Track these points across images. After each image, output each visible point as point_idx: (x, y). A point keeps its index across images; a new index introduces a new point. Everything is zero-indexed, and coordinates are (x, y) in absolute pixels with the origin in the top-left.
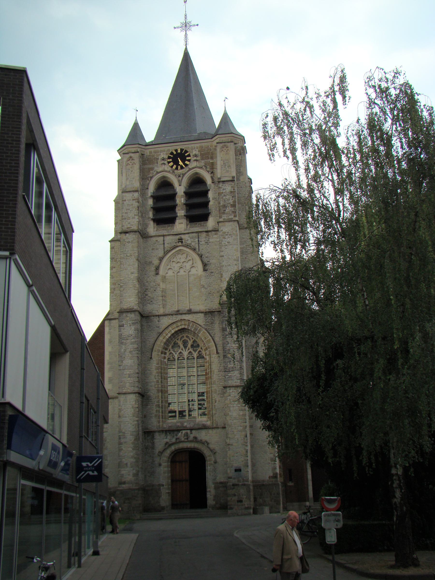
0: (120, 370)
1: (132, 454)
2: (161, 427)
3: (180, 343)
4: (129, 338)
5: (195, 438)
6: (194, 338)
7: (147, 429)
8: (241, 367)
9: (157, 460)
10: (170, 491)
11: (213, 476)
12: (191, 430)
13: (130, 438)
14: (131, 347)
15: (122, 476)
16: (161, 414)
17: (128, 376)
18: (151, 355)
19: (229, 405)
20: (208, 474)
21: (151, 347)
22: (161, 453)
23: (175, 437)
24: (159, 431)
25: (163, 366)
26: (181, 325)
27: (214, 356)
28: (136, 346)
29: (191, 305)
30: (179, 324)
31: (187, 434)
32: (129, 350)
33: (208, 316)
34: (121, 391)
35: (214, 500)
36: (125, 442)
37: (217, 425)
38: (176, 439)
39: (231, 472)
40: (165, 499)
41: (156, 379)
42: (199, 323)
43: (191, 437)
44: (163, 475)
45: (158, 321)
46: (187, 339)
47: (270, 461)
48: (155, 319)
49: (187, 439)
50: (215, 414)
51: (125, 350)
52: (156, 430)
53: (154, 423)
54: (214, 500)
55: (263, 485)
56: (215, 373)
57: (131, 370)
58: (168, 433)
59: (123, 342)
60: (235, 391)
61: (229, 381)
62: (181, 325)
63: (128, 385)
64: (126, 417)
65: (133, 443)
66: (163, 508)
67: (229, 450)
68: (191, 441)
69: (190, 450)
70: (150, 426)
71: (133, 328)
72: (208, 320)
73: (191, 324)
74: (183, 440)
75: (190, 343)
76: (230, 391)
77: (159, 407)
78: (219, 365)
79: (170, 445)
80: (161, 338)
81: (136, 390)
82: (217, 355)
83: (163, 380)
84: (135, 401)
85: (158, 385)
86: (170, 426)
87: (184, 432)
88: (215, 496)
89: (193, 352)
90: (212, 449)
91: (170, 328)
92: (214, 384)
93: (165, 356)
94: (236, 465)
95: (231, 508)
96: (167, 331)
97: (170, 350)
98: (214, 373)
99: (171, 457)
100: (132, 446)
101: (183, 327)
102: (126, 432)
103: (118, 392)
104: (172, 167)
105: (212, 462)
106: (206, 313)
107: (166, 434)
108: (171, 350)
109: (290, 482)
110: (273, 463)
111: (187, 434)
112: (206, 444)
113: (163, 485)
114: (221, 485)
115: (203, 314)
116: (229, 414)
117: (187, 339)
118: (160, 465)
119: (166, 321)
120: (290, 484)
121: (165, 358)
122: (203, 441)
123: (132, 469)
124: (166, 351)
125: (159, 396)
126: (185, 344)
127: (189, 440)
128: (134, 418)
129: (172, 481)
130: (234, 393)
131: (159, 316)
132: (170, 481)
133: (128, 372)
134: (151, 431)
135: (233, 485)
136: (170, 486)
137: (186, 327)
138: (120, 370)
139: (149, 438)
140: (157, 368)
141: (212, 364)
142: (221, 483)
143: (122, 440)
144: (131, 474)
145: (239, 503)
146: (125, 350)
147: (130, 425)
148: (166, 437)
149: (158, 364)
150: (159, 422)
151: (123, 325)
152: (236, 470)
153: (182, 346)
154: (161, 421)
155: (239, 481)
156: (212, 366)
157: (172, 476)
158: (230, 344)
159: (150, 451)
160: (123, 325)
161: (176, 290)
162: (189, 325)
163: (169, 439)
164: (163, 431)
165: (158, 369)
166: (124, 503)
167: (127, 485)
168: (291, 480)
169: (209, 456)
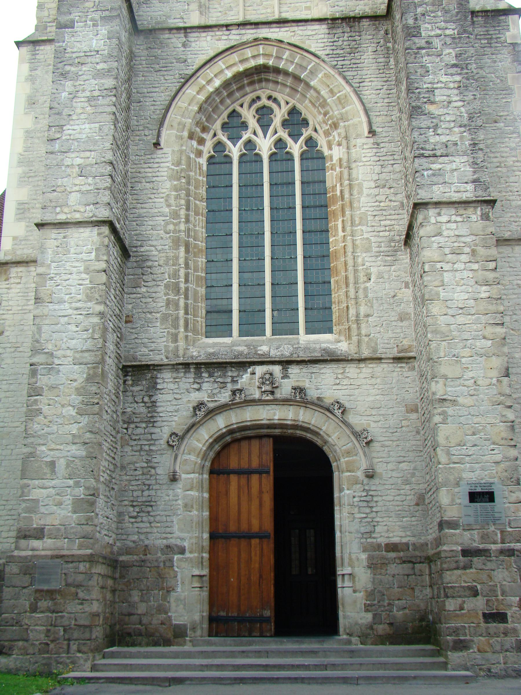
0: (52, 153)
1: (74, 429)
2: (181, 353)
3: (249, 116)
4: (89, 60)
5: (300, 390)
6: (292, 102)
7: (135, 359)
8: (475, 144)
9: (164, 463)
10: (206, 572)
11: (364, 522)
12: (286, 363)
13: (70, 374)
14: (92, 85)
15: (34, 506)
16: (182, 312)
17: (76, 170)
18: (159, 136)
19: (439, 265)
20: (345, 514)
21: (157, 116)
22: (177, 439)
23: (230, 386)
24: (175, 367)
25: (192, 174)
26: (254, 57)
27: (359, 141)
28: (109, 82)
29: (283, 10)
30: (248, 53)
31: (269, 379)
32: (88, 94)
33: (340, 31)
34: (49, 217)
35: (367, 608)
36: (52, 388)
37: (375, 351)
38: (234, 392)
39: (451, 502)
40: (187, 600)
41: (169, 206)
42: (312, 50)
43: (286, 388)
44: (182, 515)
45: (184, 45)
46: (270, 103)
48: (174, 40)
49: (271, 396)
50: (368, 316)
51: (73, 96)
52: (166, 361)
53: (157, 342)
54: (367, 608)
56: (365, 192)
57: (88, 154)
58: (205, 375)
59: (68, 72)
60: (459, 219)
61: (435, 188)
62: (254, 57)
63: (74, 198)
64: (61, 302)
65: (79, 391)
66: (179, 634)
67: (444, 422)
68: (286, 402)
69: (277, 431)
70: (145, 350)
71: (103, 31)
72: (340, 43)
73: (287, 53)
74: (257, 395)
75: (279, 114)
76: (439, 219)
77: (178, 292)
78: (377, 169)
79: (212, 413)
80: (190, 91)
81: (104, 213)
82: (371, 140)
83: (192, 213)
84: (97, 250)
85: (175, 225)
86: (213, 354)
87: (260, 370)
88: (370, 594)
89: (289, 141)
90: (358, 429)
91: (221, 64)
92: (359, 224)
93: (201, 148)
94: (475, 475)
95: (461, 645)
96: (210, 72)
97: (215, 135)
98: (360, 193)
99: (212, 454)
100: (76, 399)
101: (261, 61)
102: (59, 353)
103: (36, 221)
105: (360, 474)
106: (333, 22)
107: (198, 374)
108: (220, 133)
111: (269, 379)
112: (338, 412)
113: (182, 551)
114: (392, 555)
115: (324, 27)
116: (438, 294)
117: (270, 103)
118: (174, 479)
119: (207, 45)
121: (199, 154)
122: (328, 401)
123: (71, 482)
124: (204, 136)
125: (177, 258)
126: (264, 116)
127: (278, 395)
128: (89, 304)
129: (213, 537)
130: (454, 226)
131: (186, 30)
132: (206, 536)
133: (79, 161)
134: (147, 367)
135: (466, 553)
136: (206, 555)
137: (271, 63)
138: (52, 153)
139: (136, 389)
140: (175, 176)
141: (353, 165)
142: (392, 547)
143: (43, 381)
144: (68, 500)
145: (493, 626)
146: (73, 96)
147: (73, 328)
148: (196, 386)
149: (179, 164)
150: (175, 338)
151: (73, 22)
152: (474, 497)
153: (252, 123)
154: (181, 336)
155: (485, 538)
156: (354, 173)
157: (214, 519)
158: (434, 73)
159: (139, 431)
160: (73, 22)
162: (279, 58)
163: (210, 391)
164: (186, 365)
165: (179, 179)
166: (34, 609)
167: (48, 542)
169: (348, 453)
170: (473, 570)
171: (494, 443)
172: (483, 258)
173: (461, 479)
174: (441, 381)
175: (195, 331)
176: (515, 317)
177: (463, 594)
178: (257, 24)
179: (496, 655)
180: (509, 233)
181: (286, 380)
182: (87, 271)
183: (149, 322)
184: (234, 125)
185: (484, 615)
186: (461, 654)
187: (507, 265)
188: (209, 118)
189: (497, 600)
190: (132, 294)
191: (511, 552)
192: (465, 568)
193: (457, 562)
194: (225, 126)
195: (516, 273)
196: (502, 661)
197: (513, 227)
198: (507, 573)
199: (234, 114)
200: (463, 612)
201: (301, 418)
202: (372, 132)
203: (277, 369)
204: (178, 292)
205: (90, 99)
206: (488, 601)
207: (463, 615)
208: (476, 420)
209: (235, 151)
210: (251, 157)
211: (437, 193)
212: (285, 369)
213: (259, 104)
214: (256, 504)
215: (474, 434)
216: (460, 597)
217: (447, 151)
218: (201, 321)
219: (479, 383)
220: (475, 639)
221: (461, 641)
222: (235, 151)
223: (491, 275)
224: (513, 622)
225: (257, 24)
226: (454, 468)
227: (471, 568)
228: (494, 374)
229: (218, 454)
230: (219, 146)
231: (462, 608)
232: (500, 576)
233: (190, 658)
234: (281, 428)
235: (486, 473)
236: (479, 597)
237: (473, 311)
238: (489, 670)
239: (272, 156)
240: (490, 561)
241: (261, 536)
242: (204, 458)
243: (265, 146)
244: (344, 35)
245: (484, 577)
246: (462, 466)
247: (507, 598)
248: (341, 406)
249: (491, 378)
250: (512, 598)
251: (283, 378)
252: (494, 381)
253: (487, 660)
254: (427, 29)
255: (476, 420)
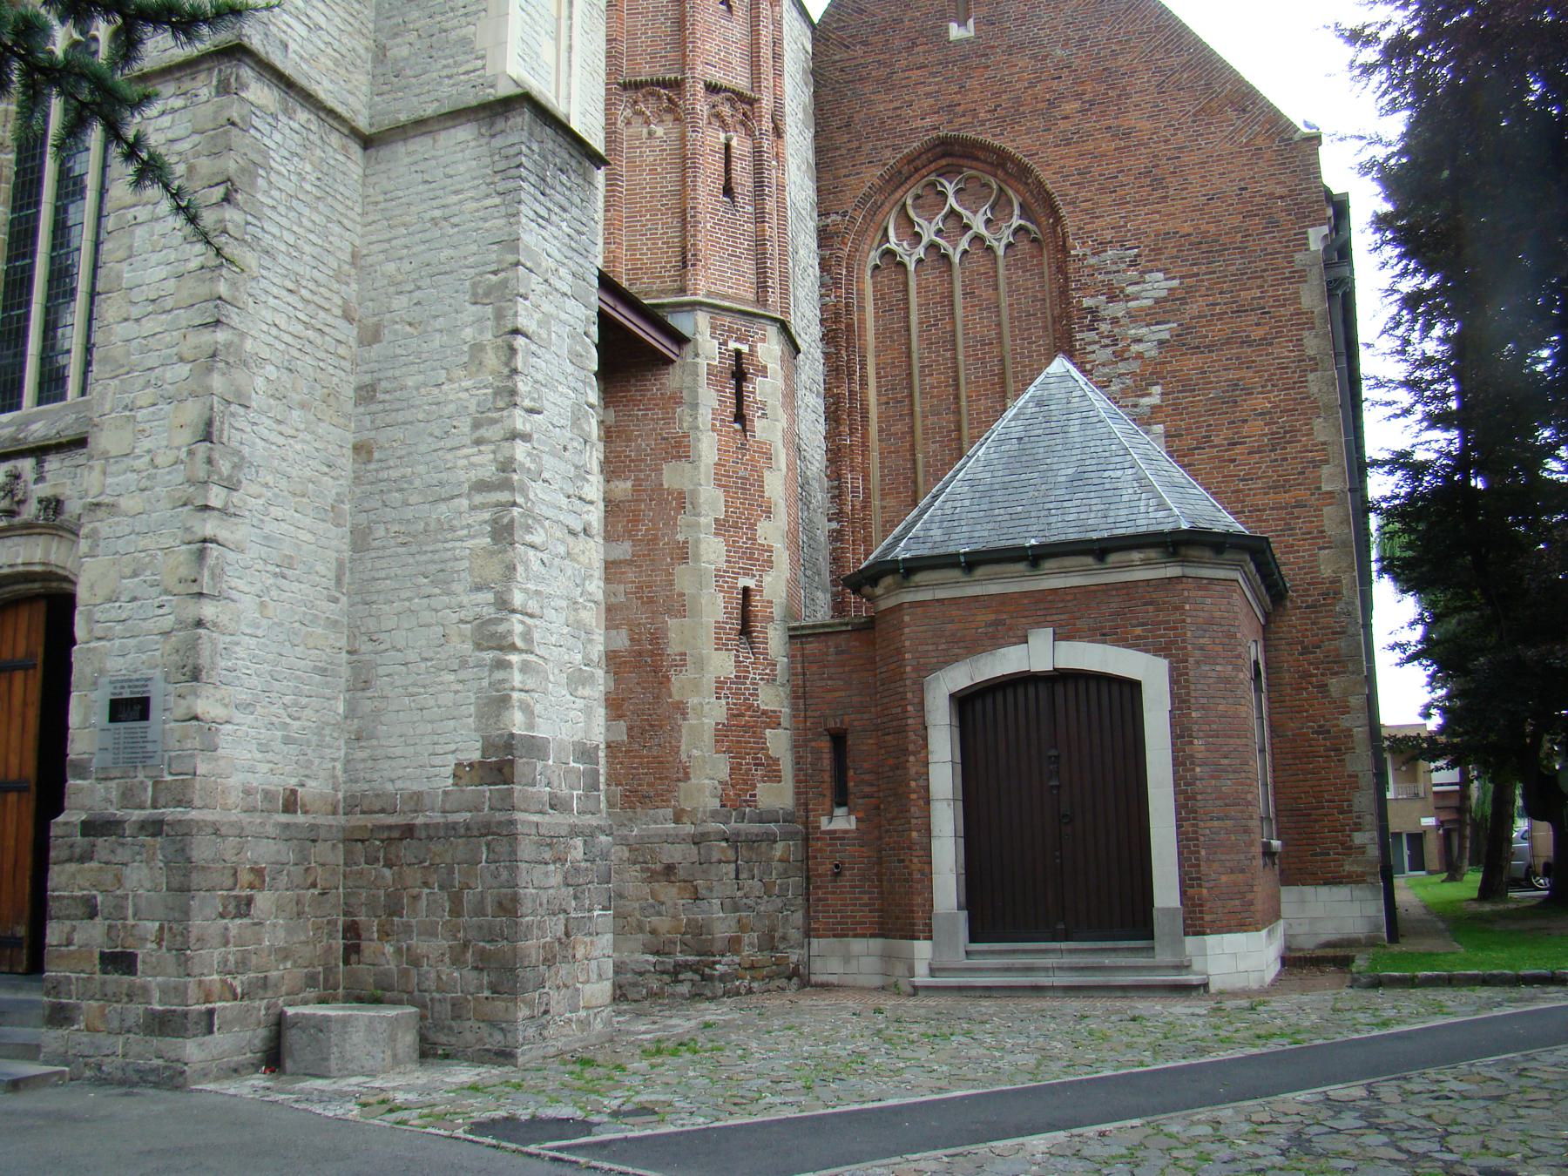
47: (468, 647)
55: (409, 831)
68: (29, 528)
109: (840, 811)
110: (488, 656)
120: (843, 821)
155: (129, 797)
161: (916, 371)
168: (841, 798)
170: (94, 864)
171: (167, 592)
172: (206, 183)
173: (102, 672)
174: (98, 464)
176: (418, 295)
177: (73, 912)
179: (112, 1039)
180: (436, 104)
181: (40, 485)
185: (102, 954)
186: (60, 1032)
187: (419, 177)
189: (124, 926)
192: (82, 859)
193: (71, 846)
195: (432, 195)
196: (120, 1052)
197: (446, 89)
198: (146, 871)
200: (72, 948)
201: (53, 558)
203: (27, 465)
206: (110, 927)
207: (73, 952)
208: (142, 543)
212: (40, 464)
215: (135, 574)
216: (68, 917)
219: (158, 461)
220: (84, 1004)
221: (62, 1007)
224: (145, 974)
226: (95, 649)
227: (92, 859)
228: (184, 437)
231: (69, 943)
232: (135, 877)
234: (44, 580)
235: (144, 657)
236: (98, 920)
237: (169, 303)
238: (99, 1067)
240: (123, 845)
241: (19, 788)
245: (108, 877)
246: (108, 644)
247: (141, 923)
249: (179, 448)
250: (149, 924)
251: (36, 481)
252: (183, 455)
253: (98, 1048)
255: (142, 543)
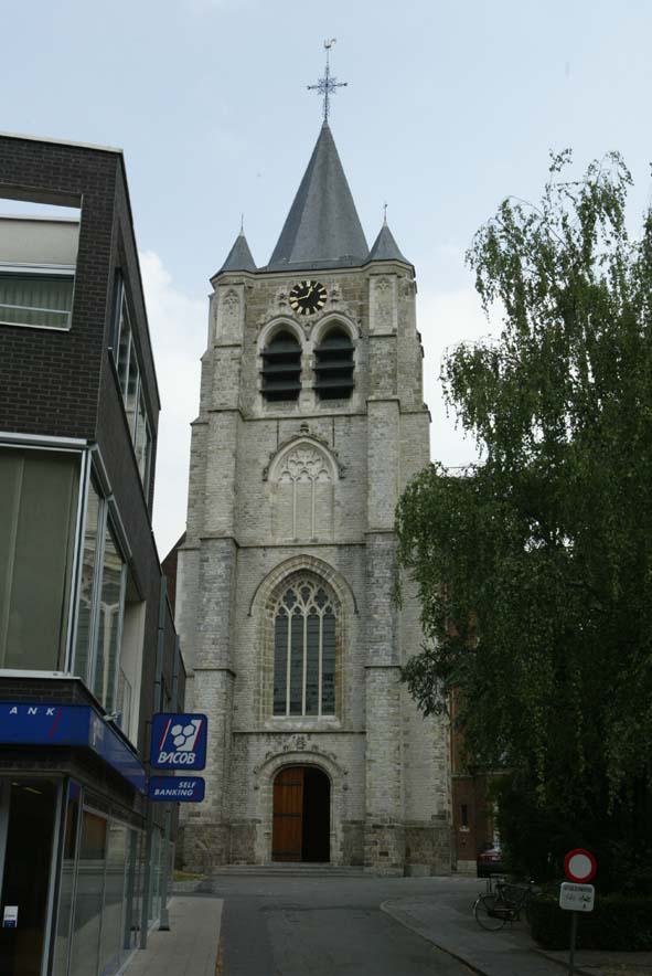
3: (298, 593)
9: (252, 781)
10: (271, 831)
11: (340, 811)
17: (211, 642)
38: (284, 748)
40: (262, 848)
53: (248, 722)
70: (243, 724)
71: (223, 564)
75: (313, 593)
77: (259, 694)
80: (267, 583)
81: (224, 665)
89: (318, 608)
101: (303, 566)
104: (296, 309)
113: (260, 822)
114: (354, 826)
119: (275, 558)
126: (306, 593)
129: (275, 815)
131: (265, 547)
134: (244, 733)
135: (374, 826)
136: (271, 824)
142: (354, 822)
146: (209, 601)
149: (260, 625)
150: (258, 719)
153: (299, 597)
175: (268, 713)
178: (301, 546)
182: (217, 693)
183: (246, 710)
184: (290, 599)
188: (277, 596)
190: (232, 603)
191: (393, 827)
194: (285, 599)
199: (290, 591)
202: (357, 612)
203: (305, 736)
204: (259, 694)
205: (217, 603)
209: (290, 613)
210: (298, 618)
211: (376, 661)
213: (302, 586)
214: (296, 803)
217: (382, 639)
218: (271, 708)
222: (290, 613)
223: (396, 702)
225: (301, 546)
228: (393, 749)
229: (278, 776)
230: (282, 610)
233: (102, 670)
239: (309, 617)
242: (271, 777)
243: (305, 611)
244: (345, 553)
248: (333, 754)
254: (377, 573)
